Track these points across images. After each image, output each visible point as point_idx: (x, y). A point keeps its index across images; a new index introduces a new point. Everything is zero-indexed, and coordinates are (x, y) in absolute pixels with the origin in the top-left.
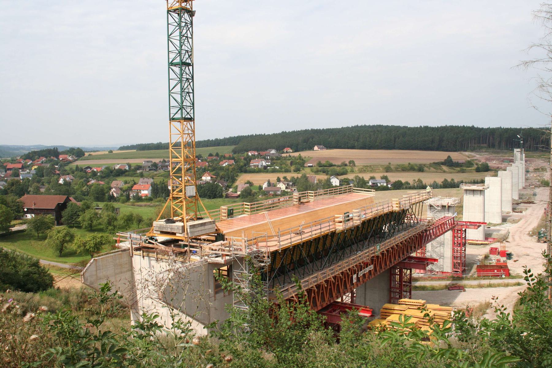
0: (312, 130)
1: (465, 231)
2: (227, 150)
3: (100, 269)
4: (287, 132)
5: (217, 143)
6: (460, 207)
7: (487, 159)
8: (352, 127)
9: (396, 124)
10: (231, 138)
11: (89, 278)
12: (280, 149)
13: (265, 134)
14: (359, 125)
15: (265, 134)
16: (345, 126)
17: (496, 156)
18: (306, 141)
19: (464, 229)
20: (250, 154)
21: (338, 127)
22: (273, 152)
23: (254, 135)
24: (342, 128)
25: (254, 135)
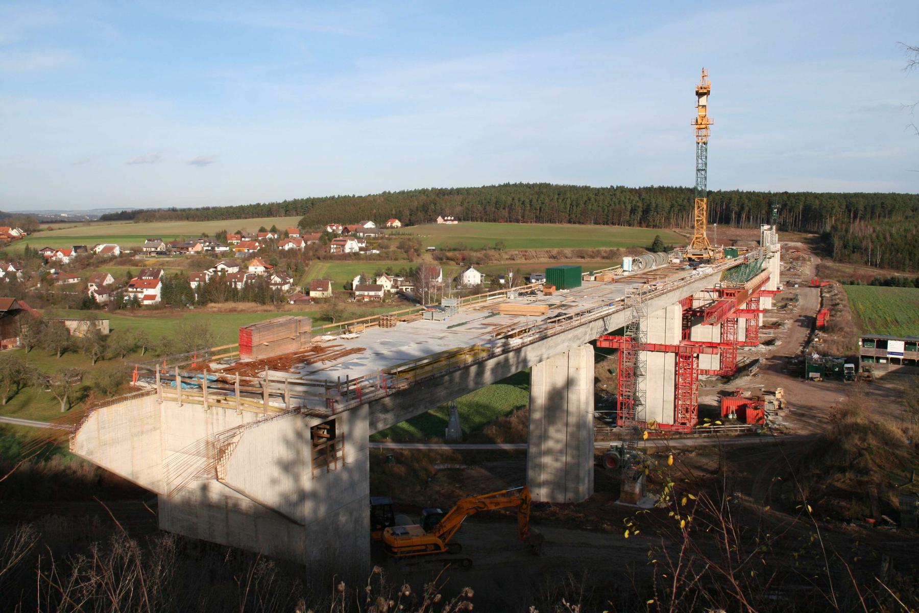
0: (434, 190)
1: (698, 357)
2: (290, 223)
3: (104, 428)
4: (392, 192)
5: (269, 210)
6: (783, 275)
7: (257, 307)
8: (500, 186)
9: (839, 192)
10: (295, 202)
11: (85, 443)
12: (380, 220)
13: (354, 196)
14: (772, 192)
15: (354, 196)
16: (488, 184)
17: (158, 313)
18: (425, 208)
19: (695, 355)
20: (329, 230)
21: (476, 186)
22: (370, 225)
23: (336, 196)
24: (484, 187)
25: (336, 196)
